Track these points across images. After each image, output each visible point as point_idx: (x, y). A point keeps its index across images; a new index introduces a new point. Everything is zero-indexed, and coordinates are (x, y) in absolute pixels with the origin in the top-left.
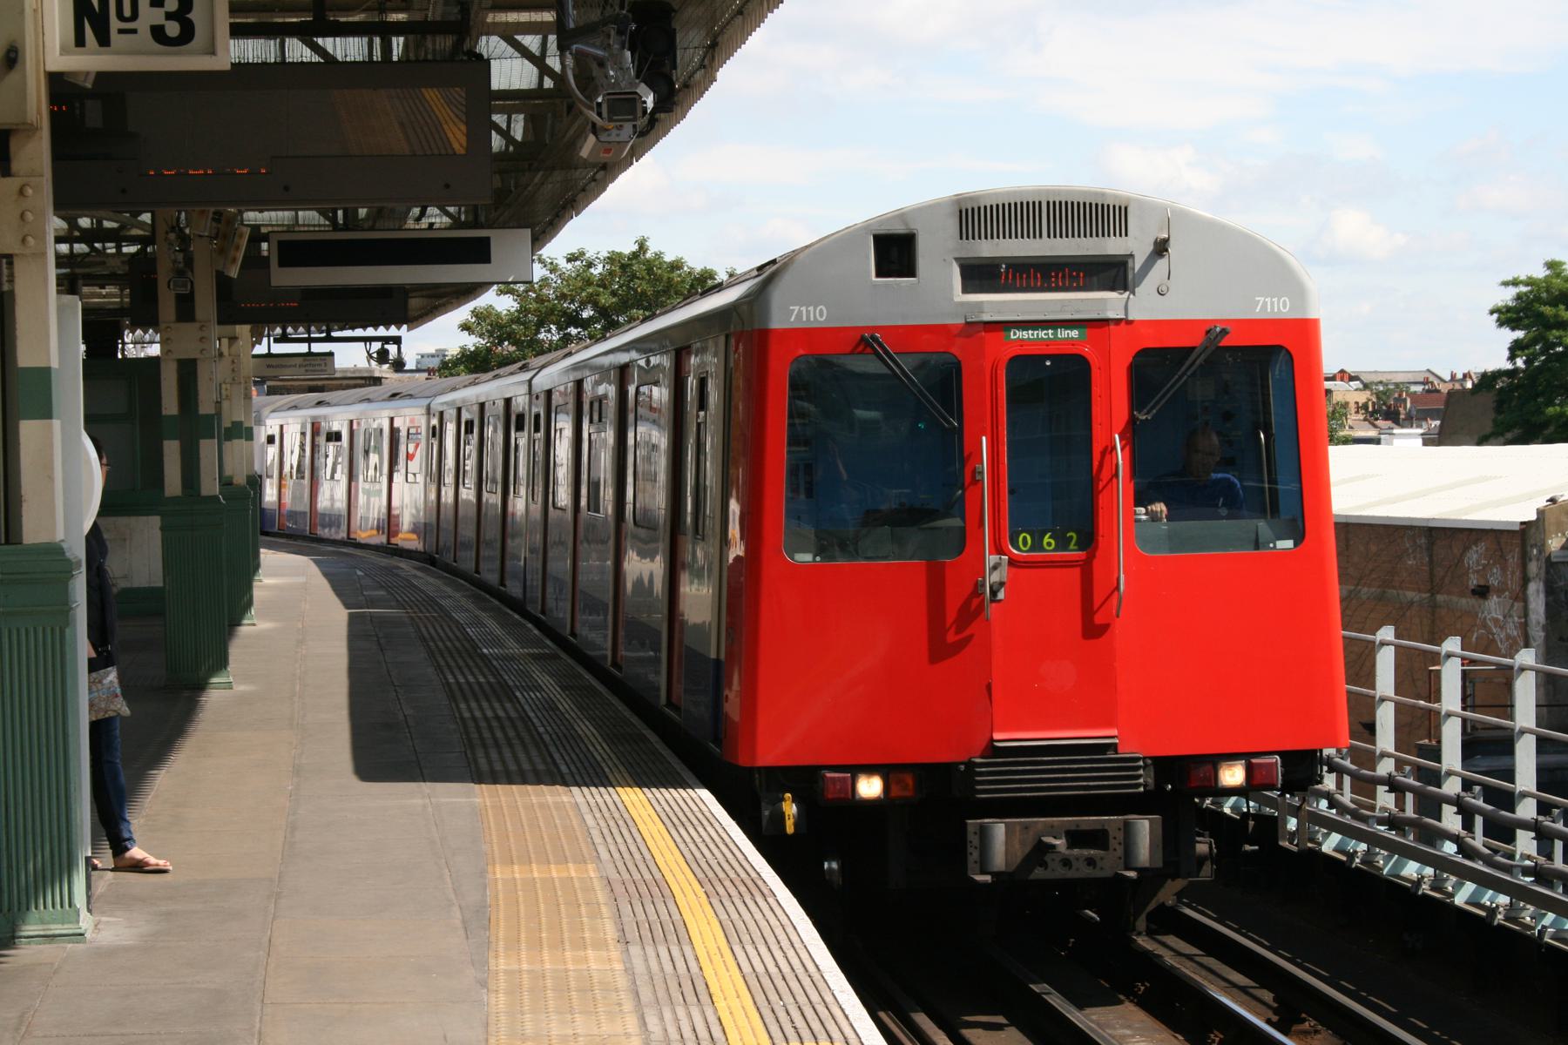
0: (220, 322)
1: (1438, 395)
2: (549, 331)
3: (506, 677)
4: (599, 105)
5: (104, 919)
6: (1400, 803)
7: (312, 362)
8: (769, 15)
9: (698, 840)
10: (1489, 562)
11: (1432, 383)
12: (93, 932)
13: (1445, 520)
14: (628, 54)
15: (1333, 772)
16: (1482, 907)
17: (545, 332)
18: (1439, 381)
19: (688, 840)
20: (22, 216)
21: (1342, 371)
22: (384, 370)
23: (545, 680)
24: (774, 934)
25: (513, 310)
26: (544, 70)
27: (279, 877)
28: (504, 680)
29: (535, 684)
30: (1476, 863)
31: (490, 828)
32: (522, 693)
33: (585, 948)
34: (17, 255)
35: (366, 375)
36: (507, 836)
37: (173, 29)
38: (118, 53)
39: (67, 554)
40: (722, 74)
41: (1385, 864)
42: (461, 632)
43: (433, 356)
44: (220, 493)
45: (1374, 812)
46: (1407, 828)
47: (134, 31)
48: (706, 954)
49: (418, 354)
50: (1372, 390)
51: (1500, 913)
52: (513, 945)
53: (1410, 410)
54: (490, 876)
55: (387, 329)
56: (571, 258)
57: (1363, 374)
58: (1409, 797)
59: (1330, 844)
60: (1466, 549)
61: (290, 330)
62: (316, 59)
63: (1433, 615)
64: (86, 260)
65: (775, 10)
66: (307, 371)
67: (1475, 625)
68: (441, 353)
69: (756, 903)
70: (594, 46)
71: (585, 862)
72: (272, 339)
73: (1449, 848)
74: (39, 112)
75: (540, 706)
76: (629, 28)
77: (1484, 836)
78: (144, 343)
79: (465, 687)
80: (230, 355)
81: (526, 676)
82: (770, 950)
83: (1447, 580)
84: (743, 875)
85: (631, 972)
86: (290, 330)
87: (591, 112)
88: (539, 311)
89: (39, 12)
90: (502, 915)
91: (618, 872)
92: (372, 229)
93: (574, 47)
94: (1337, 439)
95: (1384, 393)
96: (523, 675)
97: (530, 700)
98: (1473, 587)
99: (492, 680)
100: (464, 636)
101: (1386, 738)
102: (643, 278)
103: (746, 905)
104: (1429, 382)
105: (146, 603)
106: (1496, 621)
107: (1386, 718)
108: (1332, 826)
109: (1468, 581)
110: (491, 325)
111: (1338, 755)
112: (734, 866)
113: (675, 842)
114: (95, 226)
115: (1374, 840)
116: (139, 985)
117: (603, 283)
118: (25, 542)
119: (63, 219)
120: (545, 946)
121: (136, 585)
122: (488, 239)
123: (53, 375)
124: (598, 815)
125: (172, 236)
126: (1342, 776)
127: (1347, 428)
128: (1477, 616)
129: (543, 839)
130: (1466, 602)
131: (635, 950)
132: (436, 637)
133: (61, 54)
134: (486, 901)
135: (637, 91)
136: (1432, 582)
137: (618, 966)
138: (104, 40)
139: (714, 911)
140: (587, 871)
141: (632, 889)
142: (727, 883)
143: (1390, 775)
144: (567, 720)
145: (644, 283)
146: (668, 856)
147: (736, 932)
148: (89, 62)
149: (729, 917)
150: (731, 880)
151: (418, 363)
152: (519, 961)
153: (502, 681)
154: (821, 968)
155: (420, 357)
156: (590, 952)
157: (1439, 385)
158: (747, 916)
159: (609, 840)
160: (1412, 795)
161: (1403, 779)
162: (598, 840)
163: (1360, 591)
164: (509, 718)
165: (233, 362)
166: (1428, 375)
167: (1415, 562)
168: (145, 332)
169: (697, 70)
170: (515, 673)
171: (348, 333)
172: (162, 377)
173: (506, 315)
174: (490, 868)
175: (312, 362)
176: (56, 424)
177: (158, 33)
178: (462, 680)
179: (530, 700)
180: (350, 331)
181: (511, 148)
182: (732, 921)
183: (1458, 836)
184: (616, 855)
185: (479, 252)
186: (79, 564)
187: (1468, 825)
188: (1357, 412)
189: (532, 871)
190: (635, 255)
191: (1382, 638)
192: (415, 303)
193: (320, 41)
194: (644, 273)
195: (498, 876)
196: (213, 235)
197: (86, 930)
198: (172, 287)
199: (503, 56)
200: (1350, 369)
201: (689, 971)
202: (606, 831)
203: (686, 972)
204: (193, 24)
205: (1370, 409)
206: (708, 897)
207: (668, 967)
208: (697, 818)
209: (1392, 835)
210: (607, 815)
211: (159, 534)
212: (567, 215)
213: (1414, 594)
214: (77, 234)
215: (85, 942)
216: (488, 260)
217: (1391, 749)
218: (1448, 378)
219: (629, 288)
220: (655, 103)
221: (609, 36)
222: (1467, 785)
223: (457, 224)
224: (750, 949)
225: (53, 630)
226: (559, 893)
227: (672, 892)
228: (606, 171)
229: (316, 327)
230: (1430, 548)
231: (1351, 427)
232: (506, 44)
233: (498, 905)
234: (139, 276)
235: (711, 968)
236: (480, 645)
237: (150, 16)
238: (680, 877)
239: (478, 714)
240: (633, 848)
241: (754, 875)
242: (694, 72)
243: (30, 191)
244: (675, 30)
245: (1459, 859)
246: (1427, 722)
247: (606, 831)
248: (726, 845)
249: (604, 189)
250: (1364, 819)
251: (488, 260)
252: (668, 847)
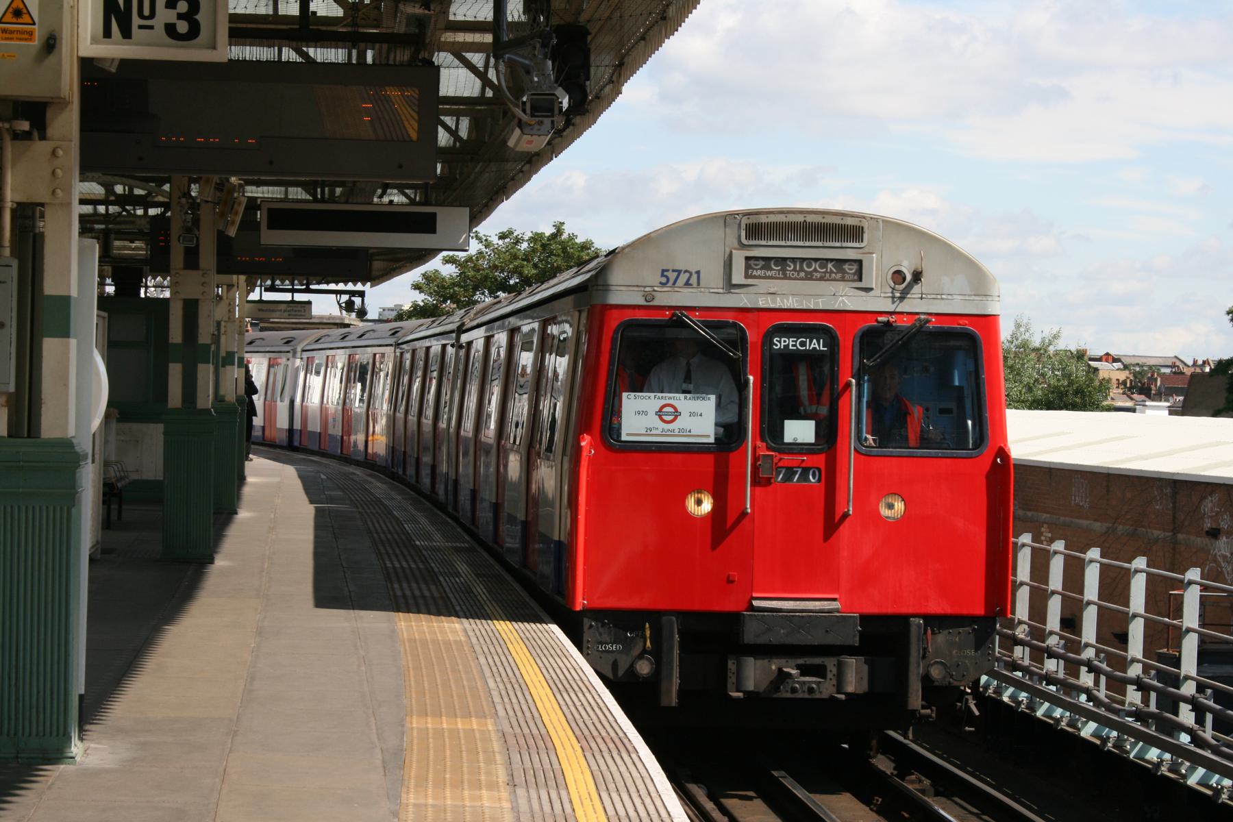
0: (219, 272)
1: (1181, 376)
2: (483, 294)
3: (433, 565)
4: (524, 103)
5: (92, 745)
6: (1146, 701)
7: (295, 309)
8: (666, 40)
9: (578, 704)
10: (1221, 510)
11: (1178, 367)
12: (83, 756)
13: (1186, 474)
14: (550, 63)
15: (1092, 672)
16: (1209, 787)
17: (480, 294)
18: (1184, 366)
19: (570, 703)
20: (54, 173)
21: (1107, 354)
22: (351, 318)
23: (462, 567)
24: (635, 784)
25: (454, 275)
26: (486, 82)
27: (238, 718)
28: (431, 567)
29: (455, 571)
30: (1207, 751)
31: (410, 685)
32: (444, 577)
33: (480, 789)
34: (47, 204)
35: (338, 321)
36: (424, 693)
37: (183, 27)
38: (136, 44)
39: (76, 448)
40: (627, 88)
41: (1133, 750)
42: (399, 527)
43: (392, 310)
44: (212, 408)
45: (1124, 706)
46: (1150, 721)
47: (151, 27)
48: (578, 798)
49: (380, 308)
50: (1130, 370)
51: (1224, 793)
52: (422, 782)
53: (1159, 388)
54: (408, 725)
55: (355, 285)
56: (503, 236)
57: (1124, 358)
58: (1153, 695)
59: (1088, 730)
60: (1203, 498)
61: (278, 282)
62: (299, 60)
63: (1174, 549)
64: (118, 219)
65: (671, 37)
66: (289, 315)
67: (1208, 559)
68: (398, 308)
69: (622, 757)
70: (522, 56)
71: (485, 717)
72: (263, 288)
73: (1185, 738)
74: (71, 89)
75: (458, 589)
76: (552, 43)
77: (1213, 730)
78: (163, 287)
79: (400, 571)
80: (227, 298)
81: (449, 564)
82: (630, 797)
83: (1186, 523)
84: (613, 734)
85: (516, 810)
86: (278, 282)
87: (517, 109)
88: (476, 278)
89: (75, 8)
90: (414, 759)
91: (512, 727)
92: (347, 202)
93: (507, 56)
94: (1102, 407)
95: (1140, 373)
96: (446, 564)
97: (450, 584)
98: (1207, 529)
99: (421, 566)
100: (402, 530)
101: (1136, 647)
102: (559, 255)
103: (613, 759)
104: (1176, 367)
105: (149, 492)
106: (1224, 557)
107: (1136, 631)
108: (1092, 716)
109: (1203, 524)
110: (438, 287)
111: (1097, 659)
112: (606, 726)
113: (559, 704)
114: (127, 193)
115: (1123, 729)
116: (115, 802)
117: (527, 257)
118: (42, 437)
119: (102, 185)
120: (448, 785)
121: (145, 477)
122: (435, 214)
123: (73, 303)
124: (498, 680)
125: (184, 200)
126: (1099, 677)
127: (1109, 399)
128: (1209, 552)
129: (452, 697)
130: (1202, 541)
131: (521, 792)
132: (379, 530)
133: (91, 44)
134: (403, 745)
135: (556, 93)
136: (1175, 523)
137: (507, 805)
138: (126, 33)
139: (588, 763)
140: (486, 724)
141: (522, 741)
142: (599, 740)
143: (1138, 677)
144: (479, 600)
145: (559, 259)
146: (553, 715)
147: (604, 781)
148: (115, 50)
149: (599, 768)
150: (602, 738)
151: (380, 315)
152: (426, 796)
153: (429, 567)
154: (671, 814)
155: (382, 310)
156: (484, 792)
157: (1183, 368)
158: (613, 768)
159: (506, 700)
160: (1029, 648)
161: (1205, 701)
162: (497, 699)
163: (1116, 529)
164: (433, 598)
165: (230, 304)
166: (1175, 360)
167: (1161, 507)
168: (164, 279)
169: (607, 84)
170: (439, 561)
171: (324, 287)
172: (171, 312)
173: (449, 279)
174: (408, 719)
175: (295, 309)
176: (73, 342)
177: (170, 29)
178: (397, 565)
179: (450, 584)
180: (326, 285)
181: (458, 144)
182: (601, 772)
183: (1192, 729)
184: (511, 713)
185: (427, 224)
186: (86, 456)
187: (1200, 720)
188: (1118, 387)
189: (441, 723)
190: (554, 236)
191: (1136, 566)
192: (377, 265)
194: (560, 252)
195: (414, 725)
196: (216, 202)
197: (76, 755)
198: (181, 241)
199: (452, 65)
200: (1113, 352)
201: (564, 812)
202: (504, 693)
203: (561, 812)
204: (199, 25)
205: (1128, 385)
206: (583, 751)
207: (547, 808)
208: (578, 685)
209: (1138, 725)
210: (506, 680)
211: (162, 436)
212: (499, 200)
213: (1159, 532)
214: (112, 198)
215: (75, 764)
216: (434, 231)
217: (1140, 656)
218: (1190, 363)
219: (548, 263)
220: (569, 105)
221: (535, 48)
222: (1201, 688)
223: (413, 202)
224: (615, 795)
225: (61, 509)
226: (463, 742)
227: (554, 745)
228: (534, 161)
229: (299, 281)
231: (1112, 399)
232: (453, 57)
233: (412, 750)
234: (157, 231)
235: (582, 810)
236: (415, 539)
237: (165, 15)
238: (562, 733)
239: (408, 593)
240: (525, 708)
241: (621, 734)
242: (605, 86)
243: (60, 152)
244: (589, 49)
245: (1192, 747)
246: (1166, 636)
247: (504, 693)
248: (600, 709)
249: (529, 179)
250: (1116, 712)
251: (434, 231)
252: (553, 708)
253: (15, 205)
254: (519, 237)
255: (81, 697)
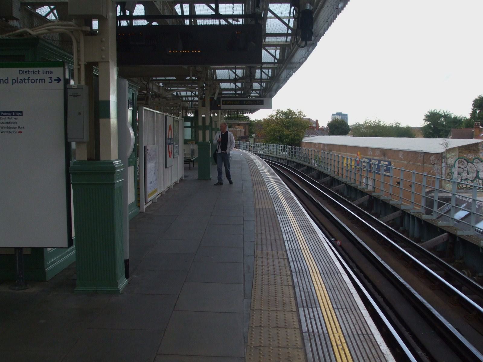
3: (264, 179)
7: (33, 76)
8: (283, 111)
60: (430, 157)
118: (101, 160)
175: (33, 76)
193: (227, 24)
230: (424, 156)
249: (286, 82)
253: (86, 63)
254: (276, 130)
255: (126, 262)
